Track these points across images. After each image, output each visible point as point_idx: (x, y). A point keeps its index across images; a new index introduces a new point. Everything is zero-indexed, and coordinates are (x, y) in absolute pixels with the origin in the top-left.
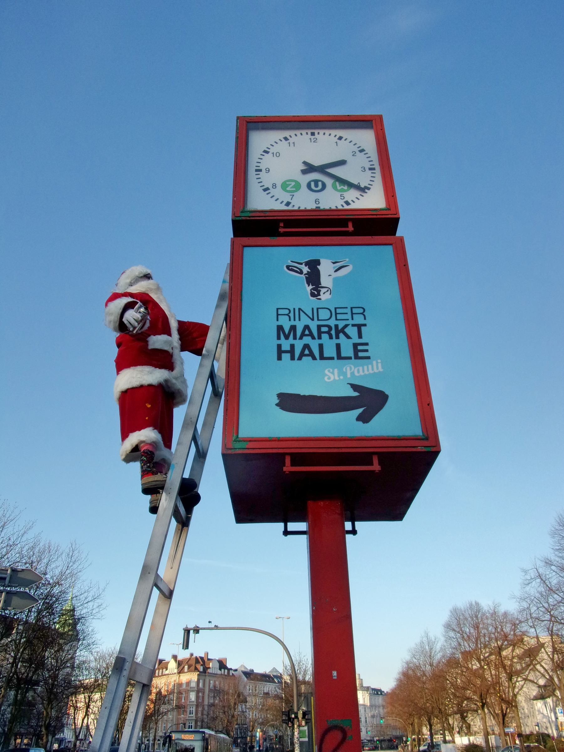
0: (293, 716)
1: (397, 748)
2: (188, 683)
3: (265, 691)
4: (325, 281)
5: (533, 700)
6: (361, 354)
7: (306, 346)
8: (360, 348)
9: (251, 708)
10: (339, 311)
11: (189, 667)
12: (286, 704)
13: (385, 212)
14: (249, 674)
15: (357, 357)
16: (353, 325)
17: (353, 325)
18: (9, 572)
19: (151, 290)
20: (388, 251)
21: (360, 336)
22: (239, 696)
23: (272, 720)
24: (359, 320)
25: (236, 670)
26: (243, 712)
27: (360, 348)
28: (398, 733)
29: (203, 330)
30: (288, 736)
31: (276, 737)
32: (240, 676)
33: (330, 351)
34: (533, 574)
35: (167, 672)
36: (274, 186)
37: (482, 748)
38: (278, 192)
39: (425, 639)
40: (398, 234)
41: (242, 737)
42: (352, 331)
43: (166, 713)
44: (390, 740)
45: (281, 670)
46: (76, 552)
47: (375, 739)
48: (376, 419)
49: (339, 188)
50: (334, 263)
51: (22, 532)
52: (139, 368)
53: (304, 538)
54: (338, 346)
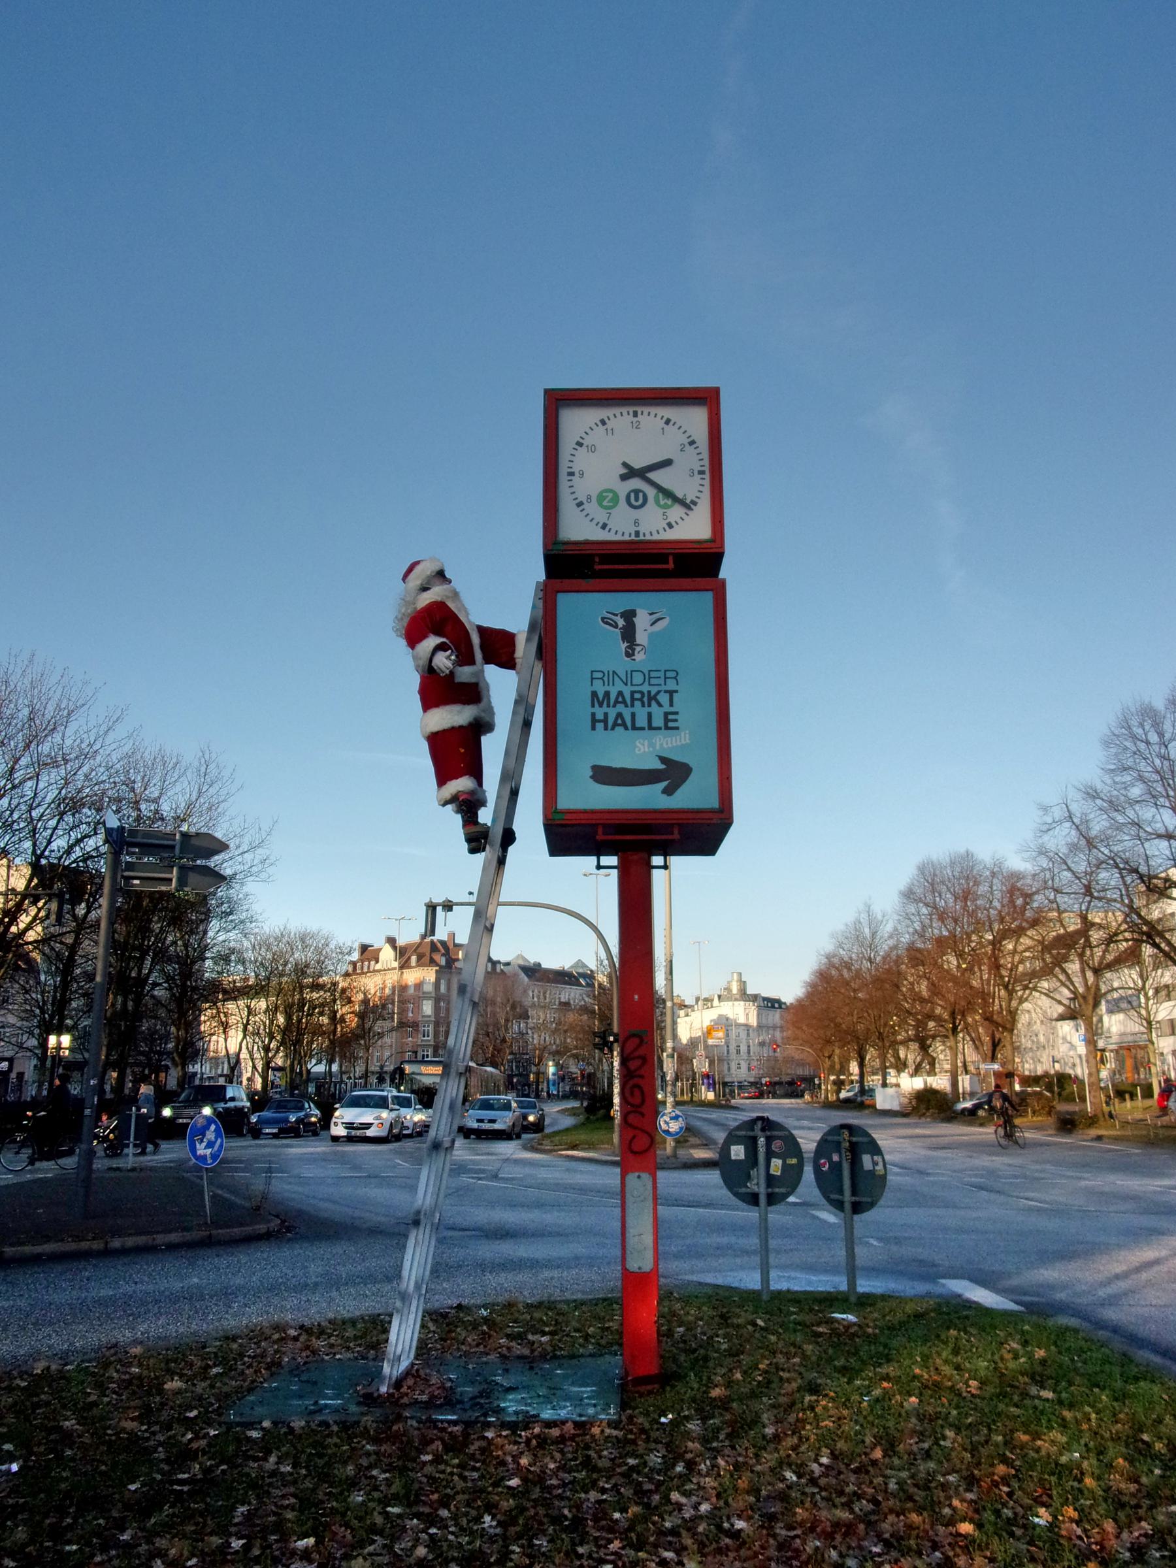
0: (612, 1039)
1: (802, 1096)
2: (419, 986)
3: (563, 1000)
4: (641, 637)
5: (1057, 1020)
6: (671, 724)
7: (619, 715)
8: (670, 717)
9: (536, 1028)
10: (652, 674)
11: (419, 958)
12: (601, 1021)
13: (711, 545)
14: (533, 971)
15: (667, 728)
16: (666, 692)
17: (666, 692)
18: (178, 837)
19: (448, 597)
20: (708, 597)
21: (671, 705)
22: (513, 1007)
23: (576, 1048)
24: (671, 685)
25: (508, 964)
26: (521, 1033)
27: (670, 717)
28: (807, 1072)
29: (507, 639)
30: (603, 1071)
31: (583, 1075)
32: (516, 975)
33: (641, 721)
34: (1058, 813)
35: (378, 967)
36: (589, 498)
37: (946, 1094)
38: (592, 508)
39: (864, 916)
40: (721, 576)
41: (520, 1075)
42: (664, 698)
43: (381, 1035)
44: (791, 1083)
45: (592, 965)
46: (212, 766)
47: (764, 1081)
48: (680, 793)
49: (662, 503)
50: (651, 614)
51: (104, 727)
52: (448, 708)
53: (616, 871)
54: (650, 715)
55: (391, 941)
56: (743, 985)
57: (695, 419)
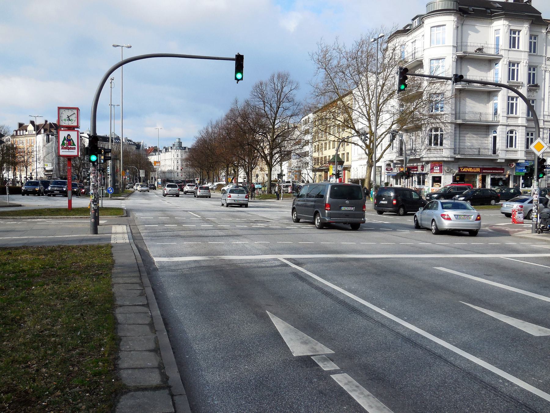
35: (27, 133)
38: (63, 121)
55: (32, 123)
56: (180, 143)
57: (75, 111)
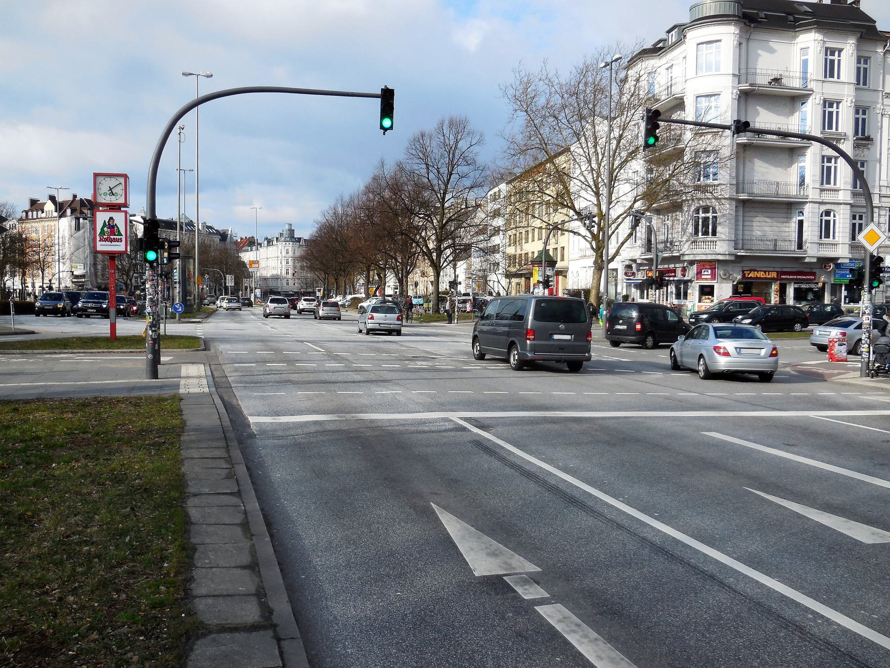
35: (44, 215)
38: (103, 195)
55: (52, 199)
56: (292, 232)
57: (122, 180)
